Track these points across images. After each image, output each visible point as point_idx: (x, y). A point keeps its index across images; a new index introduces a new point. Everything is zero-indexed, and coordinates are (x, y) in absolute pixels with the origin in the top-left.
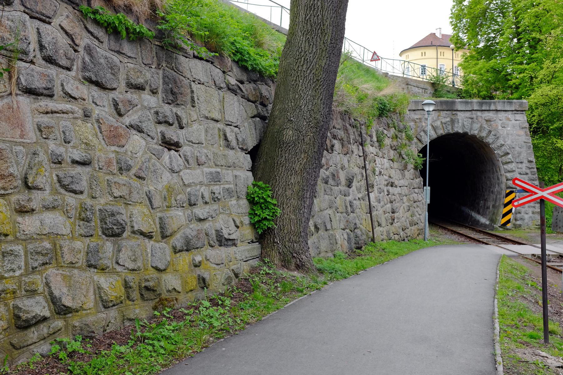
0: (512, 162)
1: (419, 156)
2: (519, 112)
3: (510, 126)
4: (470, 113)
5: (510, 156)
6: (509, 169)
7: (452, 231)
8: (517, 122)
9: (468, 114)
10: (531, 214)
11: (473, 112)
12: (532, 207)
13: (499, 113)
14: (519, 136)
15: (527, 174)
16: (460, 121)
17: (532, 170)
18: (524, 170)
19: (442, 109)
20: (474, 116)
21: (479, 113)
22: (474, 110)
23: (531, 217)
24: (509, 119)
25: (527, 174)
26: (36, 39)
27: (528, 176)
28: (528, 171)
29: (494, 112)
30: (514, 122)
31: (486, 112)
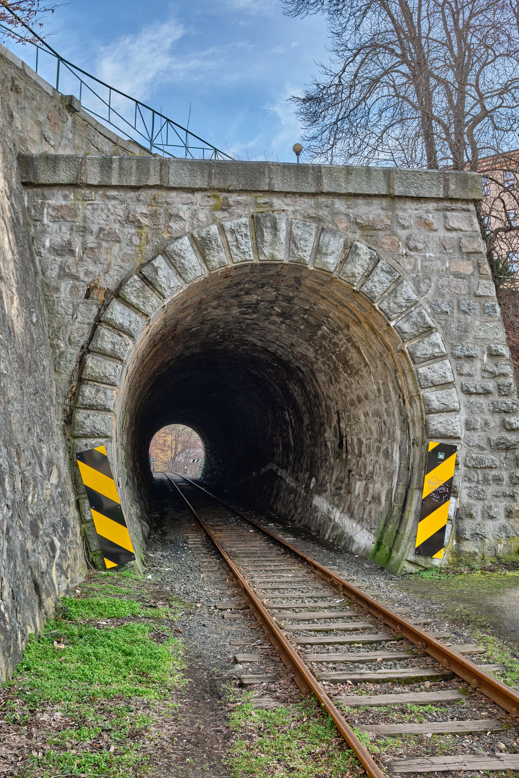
0: (443, 357)
1: (483, 377)
2: (459, 205)
3: (432, 245)
4: (312, 201)
5: (437, 337)
6: (436, 378)
7: (347, 591)
8: (454, 234)
9: (305, 205)
10: (502, 520)
11: (322, 200)
12: (505, 495)
13: (399, 204)
14: (457, 275)
15: (487, 393)
16: (283, 226)
17: (501, 380)
18: (477, 382)
19: (222, 185)
20: (323, 213)
21: (339, 205)
22: (322, 193)
23: (504, 528)
24: (428, 226)
25: (487, 393)
26: (236, 194)
27: (491, 398)
28: (491, 385)
29: (385, 202)
30: (442, 233)
31: (360, 201)
